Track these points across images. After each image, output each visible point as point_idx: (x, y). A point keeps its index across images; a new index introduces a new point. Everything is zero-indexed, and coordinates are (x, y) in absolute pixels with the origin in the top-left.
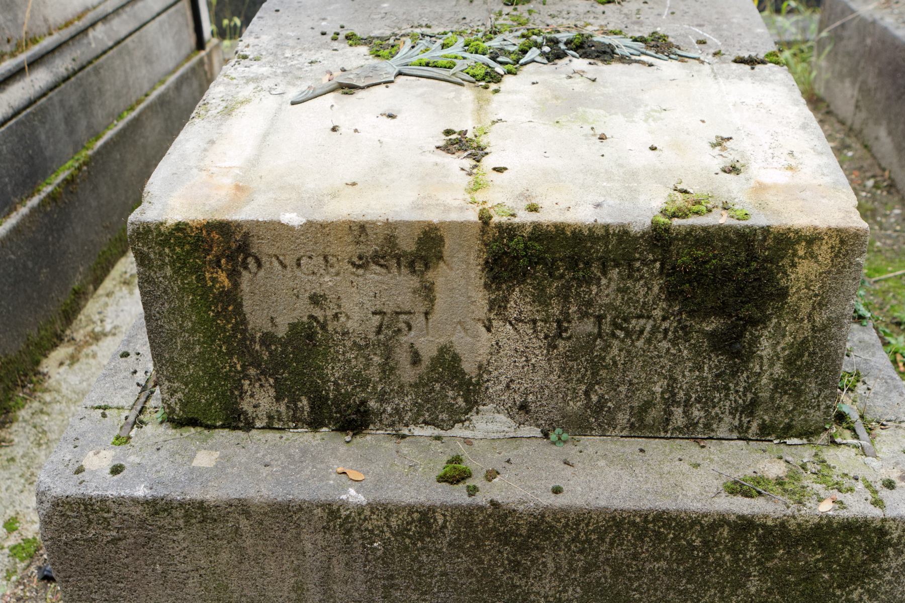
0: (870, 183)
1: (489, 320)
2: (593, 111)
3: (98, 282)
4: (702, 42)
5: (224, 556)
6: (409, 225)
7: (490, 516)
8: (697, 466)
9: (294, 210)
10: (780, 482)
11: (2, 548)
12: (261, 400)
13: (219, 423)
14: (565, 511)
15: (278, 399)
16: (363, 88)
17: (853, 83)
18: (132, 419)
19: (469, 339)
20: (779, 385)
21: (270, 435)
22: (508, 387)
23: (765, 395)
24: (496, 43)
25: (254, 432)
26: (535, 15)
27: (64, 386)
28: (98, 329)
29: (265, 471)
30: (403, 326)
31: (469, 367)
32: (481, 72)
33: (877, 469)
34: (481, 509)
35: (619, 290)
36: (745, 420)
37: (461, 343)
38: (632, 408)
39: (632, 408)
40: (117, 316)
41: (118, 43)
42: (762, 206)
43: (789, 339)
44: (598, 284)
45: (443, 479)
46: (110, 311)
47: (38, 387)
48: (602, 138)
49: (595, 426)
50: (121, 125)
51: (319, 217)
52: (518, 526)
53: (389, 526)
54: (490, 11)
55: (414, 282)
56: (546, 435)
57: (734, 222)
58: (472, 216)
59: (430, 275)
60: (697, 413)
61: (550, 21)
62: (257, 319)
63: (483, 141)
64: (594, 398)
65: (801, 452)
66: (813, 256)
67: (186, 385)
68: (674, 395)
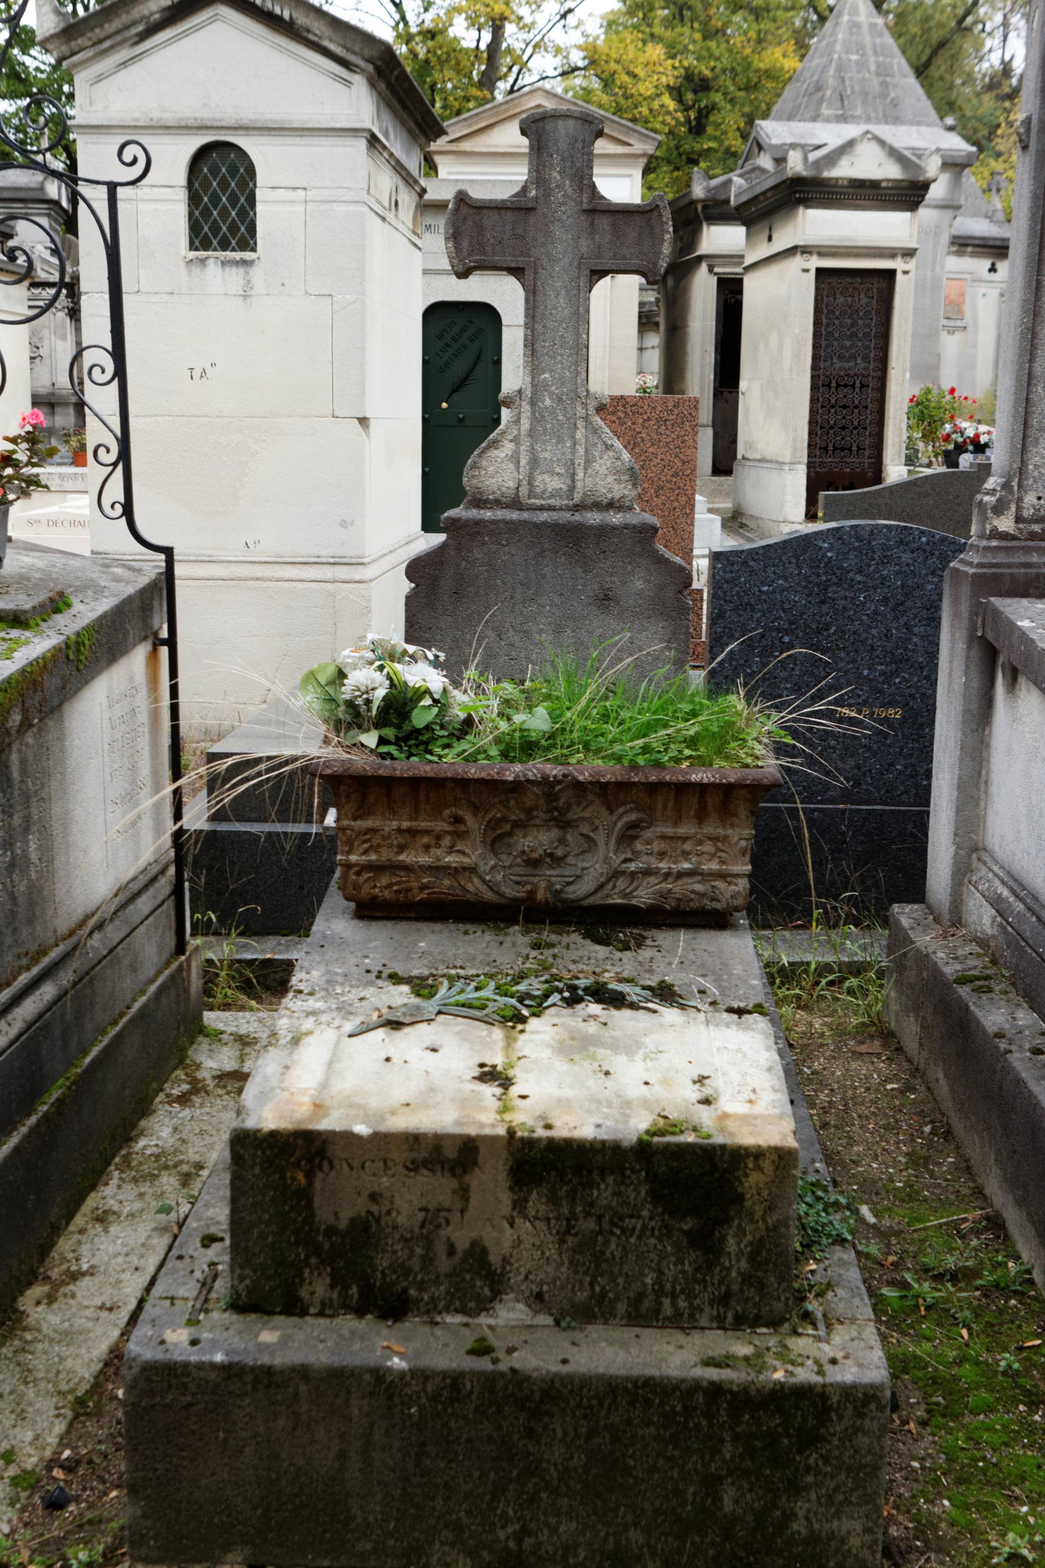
0: (927, 1129)
1: (513, 1218)
2: (602, 1051)
3: (70, 1216)
4: (702, 992)
5: (281, 1422)
6: (453, 1137)
7: (509, 1381)
8: (681, 1347)
9: (363, 1123)
10: (746, 1359)
11: (2, 1478)
12: (317, 1287)
13: (278, 1309)
14: (570, 1377)
15: (332, 1286)
16: (408, 1025)
17: (916, 1017)
18: (198, 1306)
19: (495, 1234)
20: (746, 1278)
21: (322, 1321)
22: (526, 1277)
23: (735, 1287)
24: (522, 987)
25: (308, 1318)
26: (559, 960)
27: (44, 1326)
28: (73, 1268)
29: (321, 1346)
30: (442, 1221)
31: (494, 1259)
32: (509, 1013)
33: (827, 1350)
34: (502, 1374)
35: (614, 1194)
36: (722, 1311)
37: (488, 1236)
38: (628, 1298)
39: (628, 1298)
40: (94, 1255)
41: (111, 951)
42: (722, 1130)
43: (749, 1237)
44: (599, 1188)
45: (472, 1352)
46: (85, 1249)
47: (17, 1325)
48: (607, 1073)
49: (598, 1315)
50: (106, 1041)
51: (382, 1128)
52: (532, 1391)
53: (425, 1392)
54: (519, 954)
55: (454, 1184)
56: (557, 1323)
57: (700, 1141)
58: (501, 1131)
59: (467, 1178)
60: (682, 1304)
61: (572, 967)
62: (324, 1213)
63: (511, 1073)
64: (598, 1289)
65: (768, 1338)
66: (759, 1168)
67: (255, 1271)
68: (662, 1287)
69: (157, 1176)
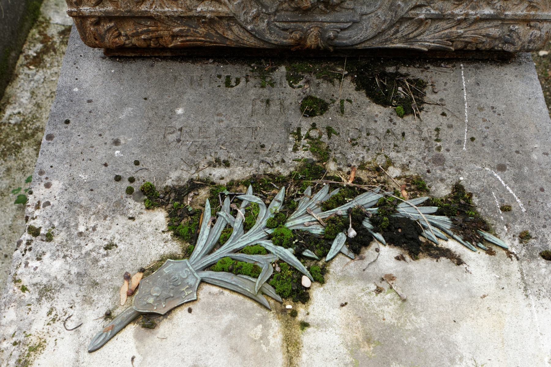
16: (166, 315)
69: (20, 147)
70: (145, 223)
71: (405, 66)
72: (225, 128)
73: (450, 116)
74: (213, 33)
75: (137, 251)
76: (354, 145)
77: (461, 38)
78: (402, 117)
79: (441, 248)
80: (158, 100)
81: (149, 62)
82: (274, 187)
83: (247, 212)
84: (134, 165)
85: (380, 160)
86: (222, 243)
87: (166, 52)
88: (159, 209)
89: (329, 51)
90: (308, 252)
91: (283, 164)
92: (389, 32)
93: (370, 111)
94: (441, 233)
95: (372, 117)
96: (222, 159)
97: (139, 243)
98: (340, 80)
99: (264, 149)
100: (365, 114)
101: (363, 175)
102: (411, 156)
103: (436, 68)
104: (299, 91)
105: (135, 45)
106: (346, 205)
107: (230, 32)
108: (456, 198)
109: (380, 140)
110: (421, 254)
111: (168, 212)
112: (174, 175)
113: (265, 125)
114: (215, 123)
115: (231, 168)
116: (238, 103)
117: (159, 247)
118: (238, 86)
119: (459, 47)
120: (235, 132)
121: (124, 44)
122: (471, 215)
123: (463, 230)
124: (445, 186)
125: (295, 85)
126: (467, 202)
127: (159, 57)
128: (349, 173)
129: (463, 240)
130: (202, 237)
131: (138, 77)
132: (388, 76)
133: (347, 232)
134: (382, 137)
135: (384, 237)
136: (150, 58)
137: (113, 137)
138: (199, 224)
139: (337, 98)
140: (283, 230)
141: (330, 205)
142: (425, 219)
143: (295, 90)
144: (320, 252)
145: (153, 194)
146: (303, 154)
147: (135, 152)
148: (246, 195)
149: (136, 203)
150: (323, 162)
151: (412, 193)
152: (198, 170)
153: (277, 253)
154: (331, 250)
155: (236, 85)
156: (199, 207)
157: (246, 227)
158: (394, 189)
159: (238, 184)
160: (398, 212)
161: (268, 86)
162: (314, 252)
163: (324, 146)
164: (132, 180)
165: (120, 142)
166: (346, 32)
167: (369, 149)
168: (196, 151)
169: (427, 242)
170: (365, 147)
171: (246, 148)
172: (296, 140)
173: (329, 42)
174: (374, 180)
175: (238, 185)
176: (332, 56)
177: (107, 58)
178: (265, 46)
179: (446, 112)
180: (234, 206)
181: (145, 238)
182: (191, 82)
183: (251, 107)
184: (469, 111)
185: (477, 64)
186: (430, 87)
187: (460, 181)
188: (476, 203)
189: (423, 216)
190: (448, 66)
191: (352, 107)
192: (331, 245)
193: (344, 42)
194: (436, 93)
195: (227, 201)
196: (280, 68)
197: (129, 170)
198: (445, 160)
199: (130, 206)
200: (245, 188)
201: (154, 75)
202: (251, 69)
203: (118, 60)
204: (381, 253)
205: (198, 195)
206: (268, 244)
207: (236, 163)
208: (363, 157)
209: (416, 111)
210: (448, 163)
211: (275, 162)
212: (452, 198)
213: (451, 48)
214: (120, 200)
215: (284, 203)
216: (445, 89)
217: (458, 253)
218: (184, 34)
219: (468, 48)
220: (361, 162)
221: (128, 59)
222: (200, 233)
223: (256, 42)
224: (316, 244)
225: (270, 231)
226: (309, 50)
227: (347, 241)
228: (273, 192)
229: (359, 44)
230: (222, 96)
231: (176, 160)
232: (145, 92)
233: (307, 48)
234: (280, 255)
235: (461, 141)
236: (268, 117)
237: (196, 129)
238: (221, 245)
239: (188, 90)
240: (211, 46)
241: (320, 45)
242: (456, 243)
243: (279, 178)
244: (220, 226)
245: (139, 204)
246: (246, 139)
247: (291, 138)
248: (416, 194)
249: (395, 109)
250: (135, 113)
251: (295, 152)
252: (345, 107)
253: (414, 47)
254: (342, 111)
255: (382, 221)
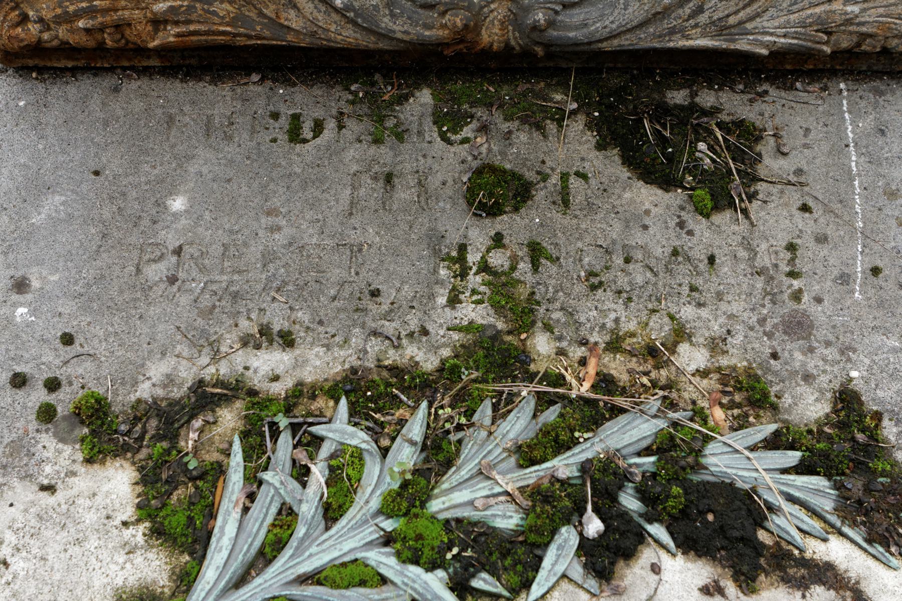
70: (80, 501)
71: (710, 88)
72: (284, 246)
73: (820, 212)
74: (253, 14)
75: (57, 576)
76: (594, 288)
77: (852, 24)
78: (707, 216)
79: (812, 560)
80: (127, 176)
81: (108, 81)
82: (401, 401)
83: (334, 477)
84: (61, 346)
85: (657, 326)
86: (269, 556)
87: (149, 57)
88: (118, 462)
89: (535, 55)
90: (484, 580)
91: (424, 339)
92: (680, 11)
93: (632, 201)
94: (806, 519)
95: (637, 217)
96: (276, 328)
97: (62, 555)
98: (560, 122)
99: (378, 299)
100: (620, 209)
101: (618, 367)
102: (731, 317)
103: (783, 94)
104: (463, 151)
105: (68, 43)
106: (576, 450)
107: (292, 13)
108: (843, 426)
109: (656, 275)
110: (762, 577)
111: (141, 469)
112: (157, 370)
113: (381, 237)
114: (261, 233)
115: (297, 352)
116: (318, 184)
117: (114, 567)
118: (318, 141)
119: (845, 45)
120: (309, 256)
121: (40, 41)
122: (884, 474)
123: (865, 515)
124: (816, 395)
125: (453, 138)
126: (871, 437)
127: (132, 68)
128: (583, 362)
129: (866, 540)
130: (218, 542)
131: (81, 117)
132: (672, 115)
133: (581, 523)
134: (660, 268)
135: (672, 534)
136: (111, 70)
137: (12, 272)
138: (213, 504)
139: (553, 169)
140: (421, 525)
141: (537, 454)
142: (772, 485)
143: (453, 149)
144: (515, 580)
145: (103, 424)
146: (472, 312)
147: (66, 310)
148: (332, 426)
149: (60, 445)
150: (520, 334)
151: (736, 412)
152: (216, 357)
153: (406, 585)
154: (542, 574)
155: (314, 138)
156: (216, 456)
157: (331, 513)
158: (694, 403)
159: (314, 393)
160: (707, 468)
161: (390, 140)
162: (499, 580)
163: (523, 292)
164: (53, 385)
165: (29, 286)
166: (576, 11)
167: (630, 299)
168: (214, 307)
169: (777, 544)
170: (620, 292)
171: (334, 299)
172: (455, 277)
173: (535, 35)
174: (645, 380)
175: (313, 397)
176: (541, 65)
177: (10, 72)
178: (381, 45)
179: (811, 203)
180: (302, 456)
181: (78, 542)
182: (208, 130)
183: (348, 192)
184: (866, 199)
185: (876, 84)
186: (772, 141)
187: (851, 380)
188: (892, 438)
189: (767, 477)
190: (810, 88)
191: (589, 192)
192: (540, 559)
193: (571, 34)
194: (784, 154)
195: (285, 440)
196: (418, 94)
197: (49, 357)
198: (811, 326)
199: (46, 454)
200: (331, 403)
201: (120, 112)
202: (351, 97)
203: (34, 75)
204: (666, 575)
205: (215, 423)
206: (383, 559)
207: (309, 339)
208: (617, 320)
209: (742, 200)
210: (822, 333)
211: (403, 333)
212: (833, 426)
213: (825, 48)
214: (20, 439)
215: (424, 448)
216: (806, 146)
217: (852, 574)
218: (182, 18)
219: (863, 48)
220: (612, 331)
221: (58, 73)
222: (216, 530)
223: (358, 36)
224: (504, 556)
225: (389, 525)
226: (487, 53)
227: (581, 547)
228: (400, 413)
229: (607, 39)
230: (280, 165)
231: (164, 330)
232: (96, 155)
233: (483, 49)
234: (415, 590)
235: (849, 276)
236: (388, 218)
237: (216, 250)
238: (269, 562)
239: (200, 151)
240: (251, 46)
241: (513, 43)
242: (848, 545)
243: (413, 378)
244: (264, 511)
245: (67, 450)
246: (336, 274)
247: (443, 272)
248: (747, 416)
249: (691, 197)
250: (69, 210)
251: (454, 308)
252: (573, 191)
253: (738, 47)
254: (564, 200)
255: (668, 497)
